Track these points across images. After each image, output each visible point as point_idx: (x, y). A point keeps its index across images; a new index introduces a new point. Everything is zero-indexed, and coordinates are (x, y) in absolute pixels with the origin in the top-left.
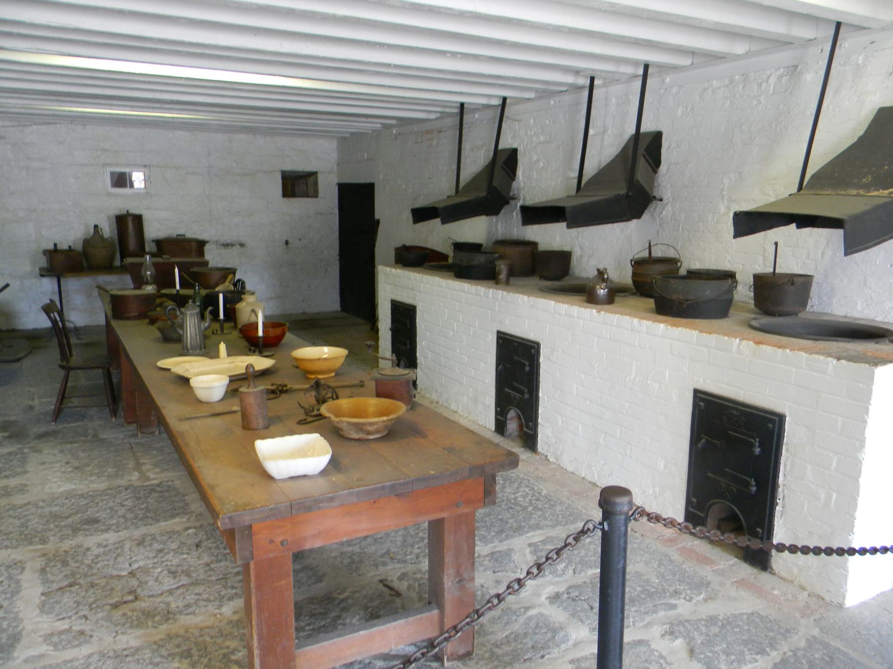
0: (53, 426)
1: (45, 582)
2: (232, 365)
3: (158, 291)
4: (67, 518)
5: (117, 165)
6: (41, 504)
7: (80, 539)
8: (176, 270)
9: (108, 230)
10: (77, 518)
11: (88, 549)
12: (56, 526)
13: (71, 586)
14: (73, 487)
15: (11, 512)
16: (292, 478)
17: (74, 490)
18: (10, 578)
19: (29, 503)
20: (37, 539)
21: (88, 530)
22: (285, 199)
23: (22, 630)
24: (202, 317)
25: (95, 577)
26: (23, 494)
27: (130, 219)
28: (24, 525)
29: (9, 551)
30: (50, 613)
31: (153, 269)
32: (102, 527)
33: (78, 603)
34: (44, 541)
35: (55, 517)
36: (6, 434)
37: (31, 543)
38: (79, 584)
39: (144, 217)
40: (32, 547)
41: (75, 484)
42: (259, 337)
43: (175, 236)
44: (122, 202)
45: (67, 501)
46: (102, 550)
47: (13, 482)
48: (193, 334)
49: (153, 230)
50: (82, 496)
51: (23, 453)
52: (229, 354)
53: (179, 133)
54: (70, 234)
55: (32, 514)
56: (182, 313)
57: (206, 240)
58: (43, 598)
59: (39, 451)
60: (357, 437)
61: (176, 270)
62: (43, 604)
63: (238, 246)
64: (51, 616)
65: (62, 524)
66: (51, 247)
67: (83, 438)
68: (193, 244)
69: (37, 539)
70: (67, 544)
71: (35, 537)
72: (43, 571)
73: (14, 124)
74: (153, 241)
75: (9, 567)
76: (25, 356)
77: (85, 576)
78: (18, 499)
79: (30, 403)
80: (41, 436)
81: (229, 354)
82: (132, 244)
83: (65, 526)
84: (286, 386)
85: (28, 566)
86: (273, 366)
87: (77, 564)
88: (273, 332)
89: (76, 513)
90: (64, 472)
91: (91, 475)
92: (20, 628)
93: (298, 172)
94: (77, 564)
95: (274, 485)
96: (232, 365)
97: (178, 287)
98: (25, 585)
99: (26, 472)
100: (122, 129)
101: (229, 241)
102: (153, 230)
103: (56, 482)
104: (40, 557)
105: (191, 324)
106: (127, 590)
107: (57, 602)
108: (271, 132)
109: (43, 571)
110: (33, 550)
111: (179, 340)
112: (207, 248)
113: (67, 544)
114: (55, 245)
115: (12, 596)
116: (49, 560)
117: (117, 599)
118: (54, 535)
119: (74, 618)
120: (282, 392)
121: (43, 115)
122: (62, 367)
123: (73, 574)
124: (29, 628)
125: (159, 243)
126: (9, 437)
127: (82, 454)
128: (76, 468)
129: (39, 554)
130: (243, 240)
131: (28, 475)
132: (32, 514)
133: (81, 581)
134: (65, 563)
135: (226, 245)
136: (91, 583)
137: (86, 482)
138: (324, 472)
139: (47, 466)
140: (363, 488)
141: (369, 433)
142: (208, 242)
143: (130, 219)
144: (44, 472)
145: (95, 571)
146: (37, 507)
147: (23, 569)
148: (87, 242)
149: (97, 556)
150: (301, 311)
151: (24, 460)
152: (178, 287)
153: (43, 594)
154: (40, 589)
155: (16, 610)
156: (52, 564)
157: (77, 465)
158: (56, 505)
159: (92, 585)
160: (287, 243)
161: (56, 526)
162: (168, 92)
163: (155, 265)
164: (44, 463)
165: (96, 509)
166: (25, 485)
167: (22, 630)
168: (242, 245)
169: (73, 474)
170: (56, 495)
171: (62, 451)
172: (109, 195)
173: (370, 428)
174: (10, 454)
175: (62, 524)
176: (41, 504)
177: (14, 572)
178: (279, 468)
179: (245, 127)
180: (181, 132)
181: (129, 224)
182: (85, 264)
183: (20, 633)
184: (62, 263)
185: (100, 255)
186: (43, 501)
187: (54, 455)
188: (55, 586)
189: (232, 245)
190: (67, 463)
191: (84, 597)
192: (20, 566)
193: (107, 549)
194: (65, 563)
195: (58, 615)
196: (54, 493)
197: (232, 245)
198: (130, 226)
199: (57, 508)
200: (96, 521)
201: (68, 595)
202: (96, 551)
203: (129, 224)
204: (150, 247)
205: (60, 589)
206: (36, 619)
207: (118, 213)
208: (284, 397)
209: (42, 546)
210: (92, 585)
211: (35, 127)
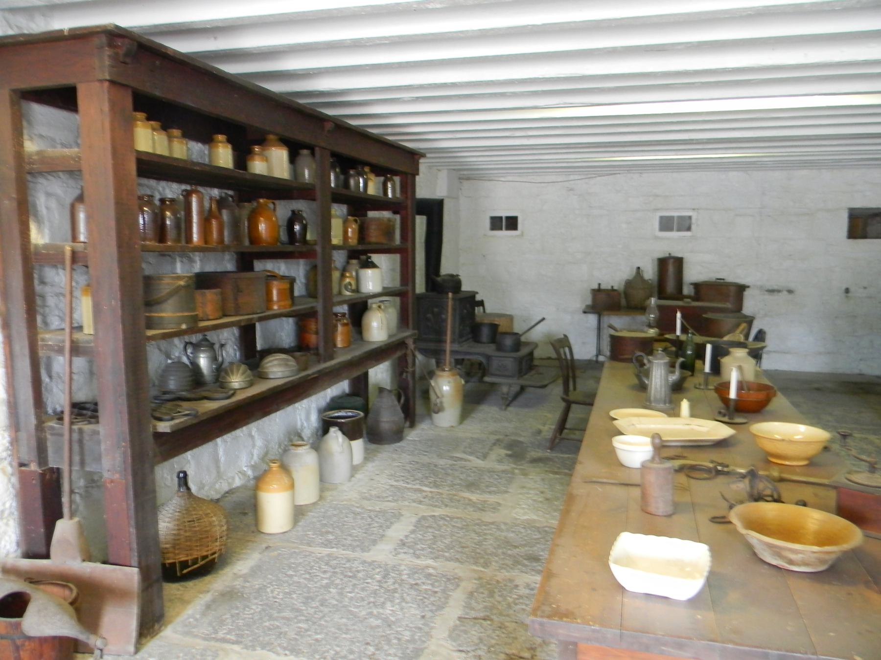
0: (548, 454)
1: (468, 606)
2: (687, 427)
3: (661, 334)
4: (516, 547)
5: (667, 210)
6: (503, 527)
7: (514, 573)
8: (679, 315)
9: (650, 273)
10: (522, 550)
11: (517, 586)
12: (503, 553)
13: (484, 619)
14: (535, 517)
15: (476, 528)
16: (648, 596)
17: (534, 521)
18: (444, 591)
19: (493, 523)
20: (482, 561)
21: (526, 566)
22: (851, 240)
23: (426, 648)
24: (672, 366)
25: (508, 619)
26: (494, 513)
27: (671, 261)
28: (479, 544)
29: (457, 564)
30: (454, 641)
31: (657, 312)
32: (539, 568)
33: (481, 640)
34: (486, 565)
35: (507, 543)
36: (509, 452)
37: (476, 563)
38: (491, 620)
39: (685, 261)
40: (476, 568)
41: (538, 516)
42: (729, 400)
43: (714, 280)
44: (673, 244)
45: (523, 531)
46: (527, 591)
47: (492, 499)
48: (658, 386)
49: (693, 274)
50: (538, 529)
51: (513, 473)
52: (693, 415)
53: (733, 175)
54: (615, 277)
55: (491, 534)
56: (649, 361)
57: (747, 284)
58: (458, 622)
59: (525, 475)
60: (774, 562)
61: (679, 315)
62: (455, 628)
63: (785, 293)
64: (454, 644)
65: (509, 552)
66: (596, 287)
67: (566, 471)
68: (732, 289)
69: (482, 561)
70: (504, 574)
71: (482, 558)
72: (471, 594)
73: (583, 177)
74: (692, 284)
75: (449, 580)
76: (550, 383)
77: (501, 614)
78: (488, 517)
79: (541, 427)
80: (535, 461)
81: (693, 415)
82: (670, 286)
83: (510, 556)
84: (727, 466)
85: (463, 584)
86: (732, 437)
87: (500, 599)
88: (754, 396)
89: (525, 545)
90: (534, 500)
91: (555, 511)
92: (426, 645)
93: (872, 209)
94: (500, 599)
95: (619, 598)
96: (687, 427)
97: (678, 332)
98: (451, 602)
99: (507, 492)
100: (675, 175)
101: (776, 287)
102: (693, 274)
103: (523, 508)
104: (475, 579)
105: (659, 374)
106: (528, 645)
107: (466, 632)
108: (837, 164)
109: (471, 594)
110: (474, 570)
111: (643, 387)
112: (747, 293)
113: (504, 574)
114: (599, 284)
115: (436, 610)
116: (481, 586)
117: (514, 651)
118: (496, 562)
119: (470, 654)
120: (719, 473)
121: (614, 166)
122: (563, 399)
123: (492, 608)
124: (433, 648)
125: (697, 286)
126: (509, 456)
127: (558, 487)
128: (547, 499)
129: (476, 576)
130: (792, 286)
131: (506, 495)
132: (491, 534)
133: (494, 617)
134: (491, 594)
135: (772, 291)
136: (502, 623)
137: (547, 516)
138: (694, 602)
139: (525, 491)
140: (730, 646)
141: (791, 562)
142: (748, 287)
143: (671, 261)
144: (520, 496)
145: (511, 612)
146: (499, 529)
147: (458, 586)
148: (629, 284)
149: (521, 597)
150: (856, 371)
151: (510, 481)
152: (678, 332)
153: (460, 618)
154: (459, 612)
155: (433, 625)
156: (481, 590)
157: (549, 496)
158: (513, 532)
159: (502, 627)
160: (847, 291)
161: (503, 553)
162: (803, 146)
163: (660, 308)
164: (523, 487)
165: (543, 547)
166: (499, 504)
167: (426, 648)
168: (790, 292)
169: (540, 505)
170: (519, 522)
171: (543, 480)
172: (657, 238)
173: (793, 556)
174: (503, 471)
175: (509, 552)
176: (503, 527)
177: (451, 587)
178: (629, 578)
179: (806, 162)
180: (735, 173)
181: (670, 267)
182: (623, 302)
183: (422, 650)
184: (604, 302)
185: (638, 294)
186: (505, 524)
187: (535, 482)
188: (473, 614)
189: (779, 291)
190: (542, 492)
191: (488, 636)
192: (456, 581)
193: (532, 592)
194: (491, 594)
195: (460, 645)
196: (517, 519)
197: (779, 291)
198: (671, 269)
199: (512, 535)
200: (535, 559)
201: (476, 628)
202: (523, 591)
203: (670, 267)
204: (687, 290)
205: (475, 618)
206: (442, 642)
207: (661, 255)
208: (721, 479)
209: (482, 569)
210: (502, 627)
211: (599, 178)
